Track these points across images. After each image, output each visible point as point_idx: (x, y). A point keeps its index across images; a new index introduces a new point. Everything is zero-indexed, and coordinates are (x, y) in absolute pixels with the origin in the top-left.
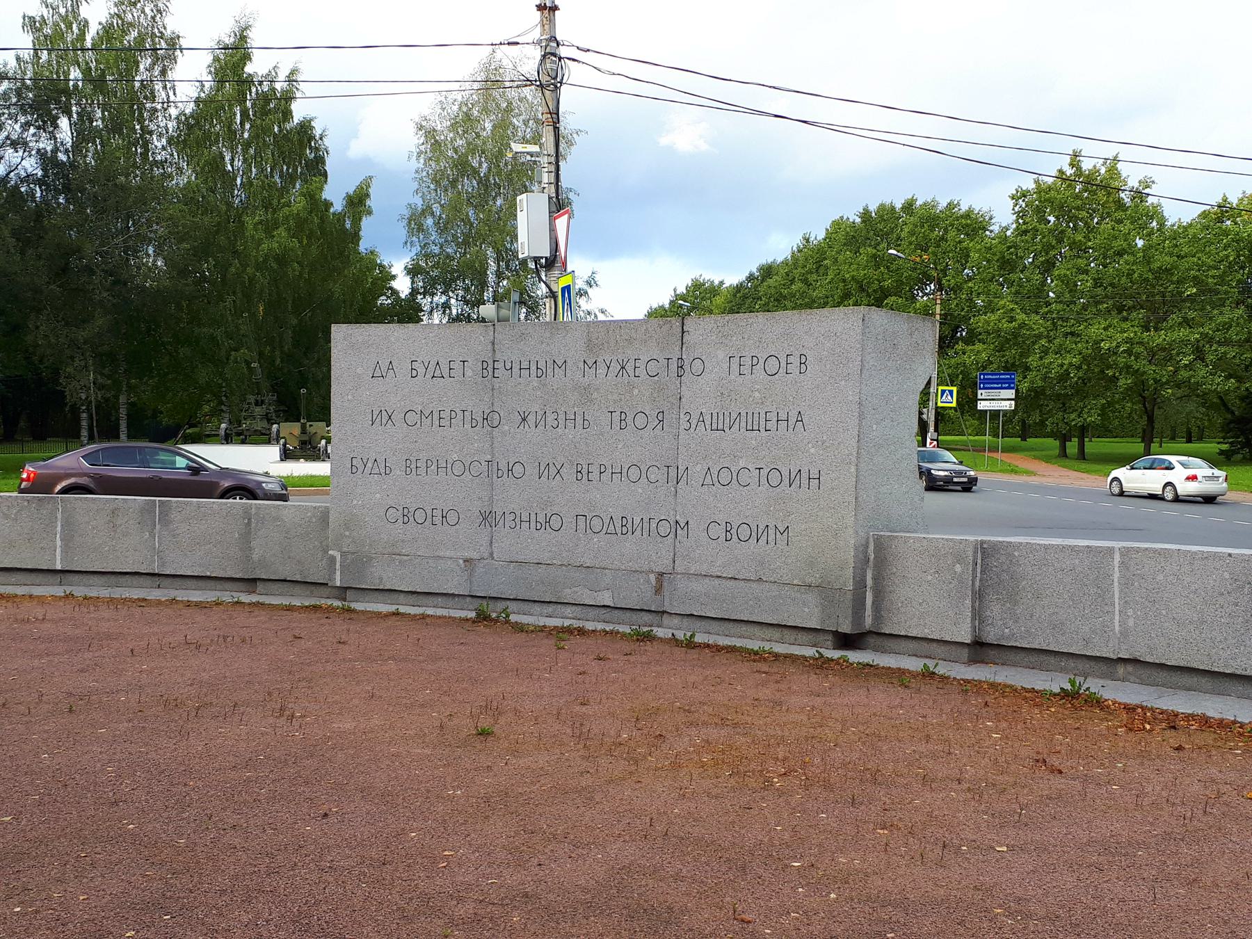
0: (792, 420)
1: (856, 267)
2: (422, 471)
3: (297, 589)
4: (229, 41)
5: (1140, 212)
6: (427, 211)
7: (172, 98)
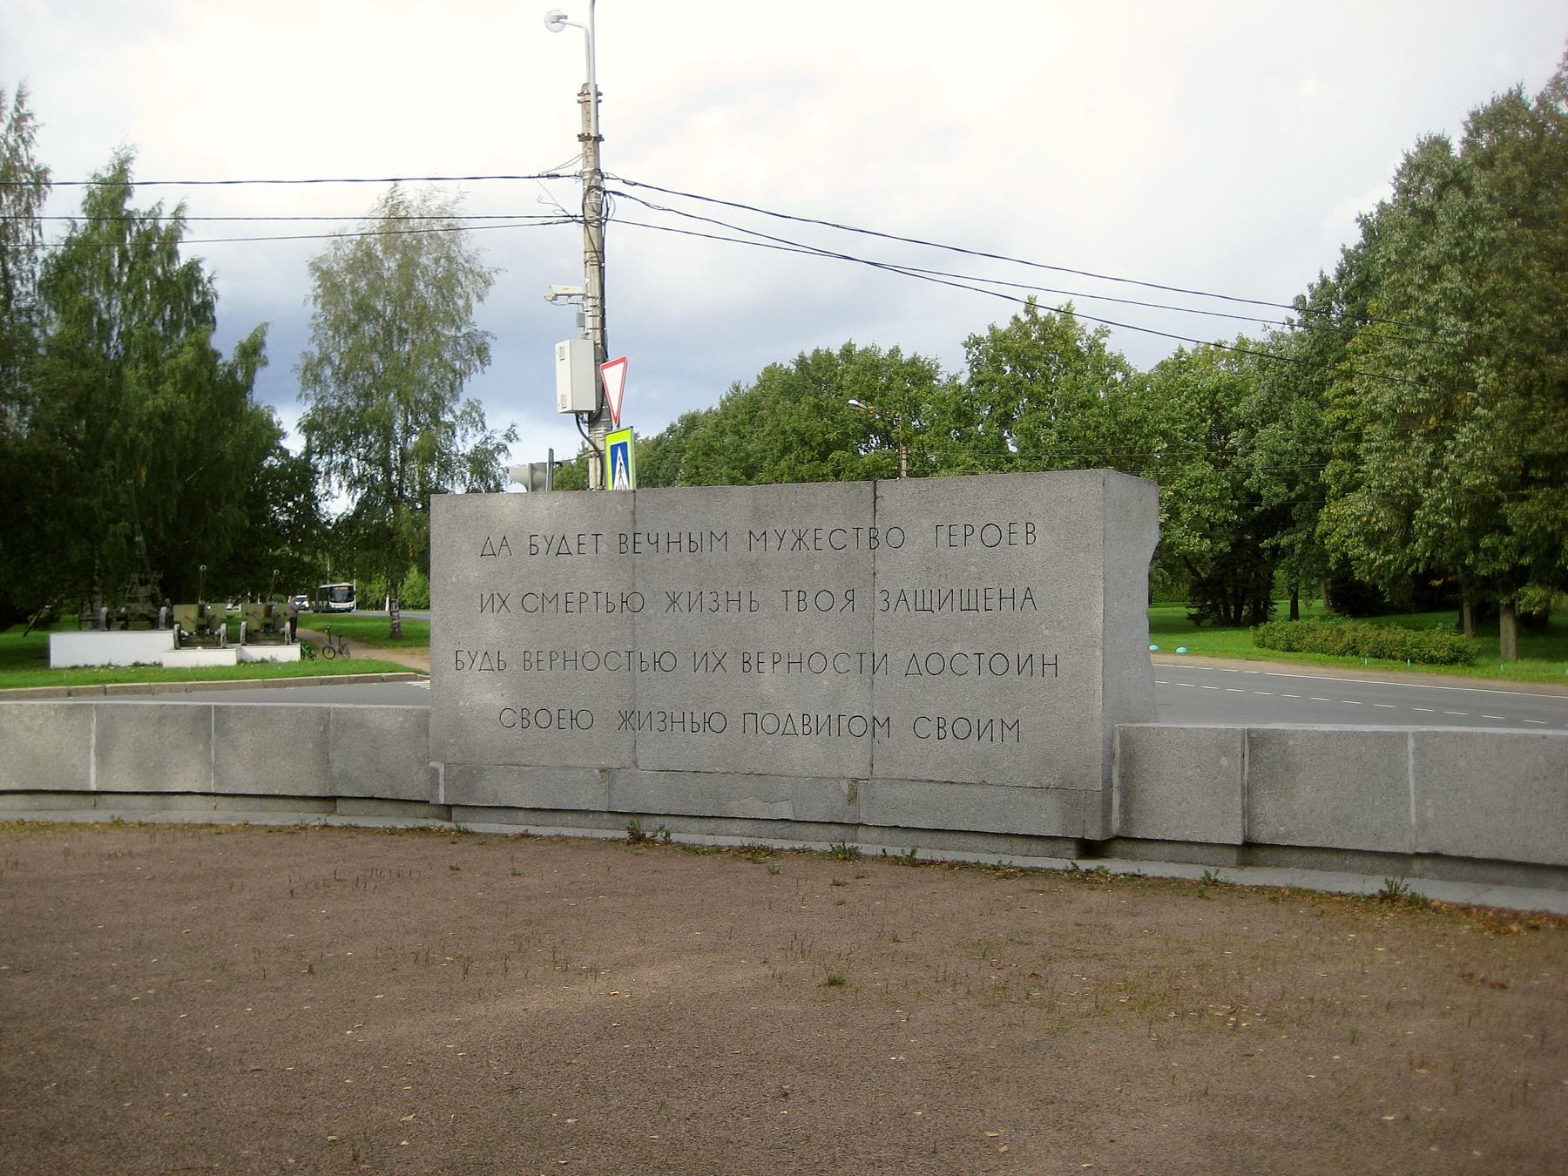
0: (1020, 597)
1: (796, 417)
2: (545, 665)
3: (387, 808)
4: (106, 175)
5: (1101, 363)
6: (325, 359)
7: (38, 238)
